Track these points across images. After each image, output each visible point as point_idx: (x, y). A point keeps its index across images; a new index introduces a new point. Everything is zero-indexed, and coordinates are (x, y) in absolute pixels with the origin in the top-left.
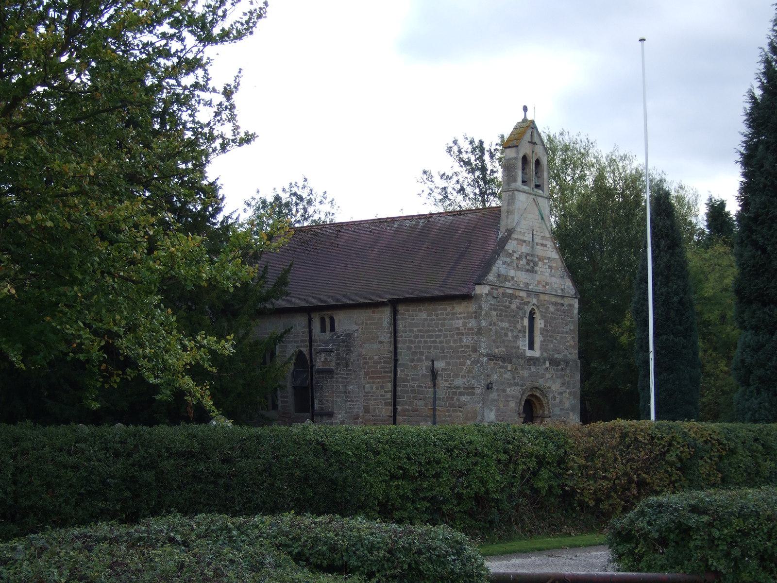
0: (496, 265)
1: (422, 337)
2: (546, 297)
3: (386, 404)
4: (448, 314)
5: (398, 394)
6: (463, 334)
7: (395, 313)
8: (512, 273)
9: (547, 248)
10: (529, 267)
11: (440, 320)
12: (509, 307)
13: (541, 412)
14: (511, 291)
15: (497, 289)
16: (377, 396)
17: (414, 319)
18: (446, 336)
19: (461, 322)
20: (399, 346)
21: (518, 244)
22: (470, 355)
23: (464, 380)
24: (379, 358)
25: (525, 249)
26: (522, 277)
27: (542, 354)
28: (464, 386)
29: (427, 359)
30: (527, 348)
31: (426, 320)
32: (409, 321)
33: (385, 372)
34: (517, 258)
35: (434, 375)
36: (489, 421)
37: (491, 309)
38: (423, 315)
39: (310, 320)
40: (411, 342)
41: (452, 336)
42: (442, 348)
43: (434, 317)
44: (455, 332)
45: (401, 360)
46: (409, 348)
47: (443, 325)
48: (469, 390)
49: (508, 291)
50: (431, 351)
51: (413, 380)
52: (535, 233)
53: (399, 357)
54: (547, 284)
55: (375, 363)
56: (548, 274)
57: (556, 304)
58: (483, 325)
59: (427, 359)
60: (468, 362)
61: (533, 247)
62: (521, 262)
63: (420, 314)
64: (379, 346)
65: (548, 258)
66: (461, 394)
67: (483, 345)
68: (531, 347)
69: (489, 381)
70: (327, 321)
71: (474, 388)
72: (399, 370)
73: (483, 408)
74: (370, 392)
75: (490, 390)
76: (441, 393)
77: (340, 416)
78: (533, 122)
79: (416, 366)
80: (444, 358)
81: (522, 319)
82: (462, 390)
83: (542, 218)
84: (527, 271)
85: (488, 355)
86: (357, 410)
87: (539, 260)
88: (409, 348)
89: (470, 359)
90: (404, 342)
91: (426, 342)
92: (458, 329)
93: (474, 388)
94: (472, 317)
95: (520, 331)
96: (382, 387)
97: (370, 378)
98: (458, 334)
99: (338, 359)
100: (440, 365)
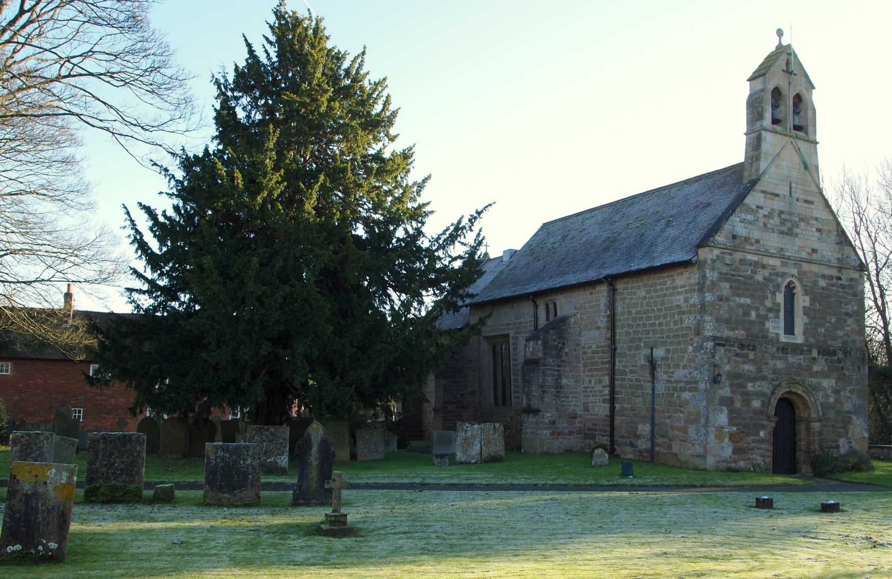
0: (729, 222)
1: (641, 319)
2: (815, 268)
3: (604, 401)
4: (668, 289)
5: (617, 389)
6: (684, 313)
7: (614, 291)
8: (756, 234)
9: (813, 206)
10: (785, 229)
11: (658, 297)
12: (751, 278)
13: (806, 414)
14: (755, 258)
15: (731, 254)
16: (596, 391)
17: (633, 295)
18: (665, 317)
19: (682, 298)
20: (617, 331)
21: (765, 197)
22: (692, 340)
23: (686, 371)
24: (597, 347)
25: (778, 205)
26: (773, 241)
27: (807, 340)
28: (685, 379)
29: (645, 347)
30: (783, 331)
31: (645, 298)
32: (627, 301)
33: (603, 363)
34: (765, 216)
35: (652, 365)
36: (716, 425)
37: (720, 280)
38: (642, 293)
39: (536, 306)
40: (629, 326)
41: (673, 315)
42: (662, 332)
43: (653, 294)
44: (675, 311)
45: (621, 347)
46: (628, 334)
47: (663, 303)
48: (692, 386)
49: (749, 257)
50: (650, 335)
51: (631, 372)
52: (793, 185)
53: (618, 345)
54: (814, 251)
55: (593, 352)
56: (816, 239)
57: (831, 277)
58: (707, 299)
59: (645, 347)
60: (690, 348)
61: (791, 204)
62: (771, 221)
63: (638, 292)
64: (597, 332)
65: (816, 219)
66: (683, 390)
67: (708, 326)
68: (789, 329)
69: (716, 372)
70: (551, 306)
71: (696, 382)
72: (617, 360)
73: (707, 408)
74: (588, 387)
75: (716, 386)
76: (660, 388)
77: (549, 415)
78: (789, 46)
79: (634, 355)
80: (664, 344)
81: (774, 293)
82: (683, 384)
83: (806, 168)
84: (782, 232)
85: (714, 338)
86: (573, 408)
87: (801, 220)
88: (628, 334)
89: (692, 345)
90: (623, 327)
91: (644, 325)
92: (679, 306)
93: (696, 382)
94: (694, 290)
95: (769, 310)
96: (600, 381)
97: (590, 370)
98: (680, 313)
99: (545, 348)
100: (659, 353)
